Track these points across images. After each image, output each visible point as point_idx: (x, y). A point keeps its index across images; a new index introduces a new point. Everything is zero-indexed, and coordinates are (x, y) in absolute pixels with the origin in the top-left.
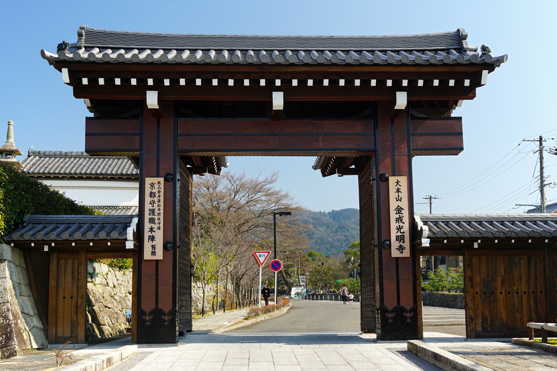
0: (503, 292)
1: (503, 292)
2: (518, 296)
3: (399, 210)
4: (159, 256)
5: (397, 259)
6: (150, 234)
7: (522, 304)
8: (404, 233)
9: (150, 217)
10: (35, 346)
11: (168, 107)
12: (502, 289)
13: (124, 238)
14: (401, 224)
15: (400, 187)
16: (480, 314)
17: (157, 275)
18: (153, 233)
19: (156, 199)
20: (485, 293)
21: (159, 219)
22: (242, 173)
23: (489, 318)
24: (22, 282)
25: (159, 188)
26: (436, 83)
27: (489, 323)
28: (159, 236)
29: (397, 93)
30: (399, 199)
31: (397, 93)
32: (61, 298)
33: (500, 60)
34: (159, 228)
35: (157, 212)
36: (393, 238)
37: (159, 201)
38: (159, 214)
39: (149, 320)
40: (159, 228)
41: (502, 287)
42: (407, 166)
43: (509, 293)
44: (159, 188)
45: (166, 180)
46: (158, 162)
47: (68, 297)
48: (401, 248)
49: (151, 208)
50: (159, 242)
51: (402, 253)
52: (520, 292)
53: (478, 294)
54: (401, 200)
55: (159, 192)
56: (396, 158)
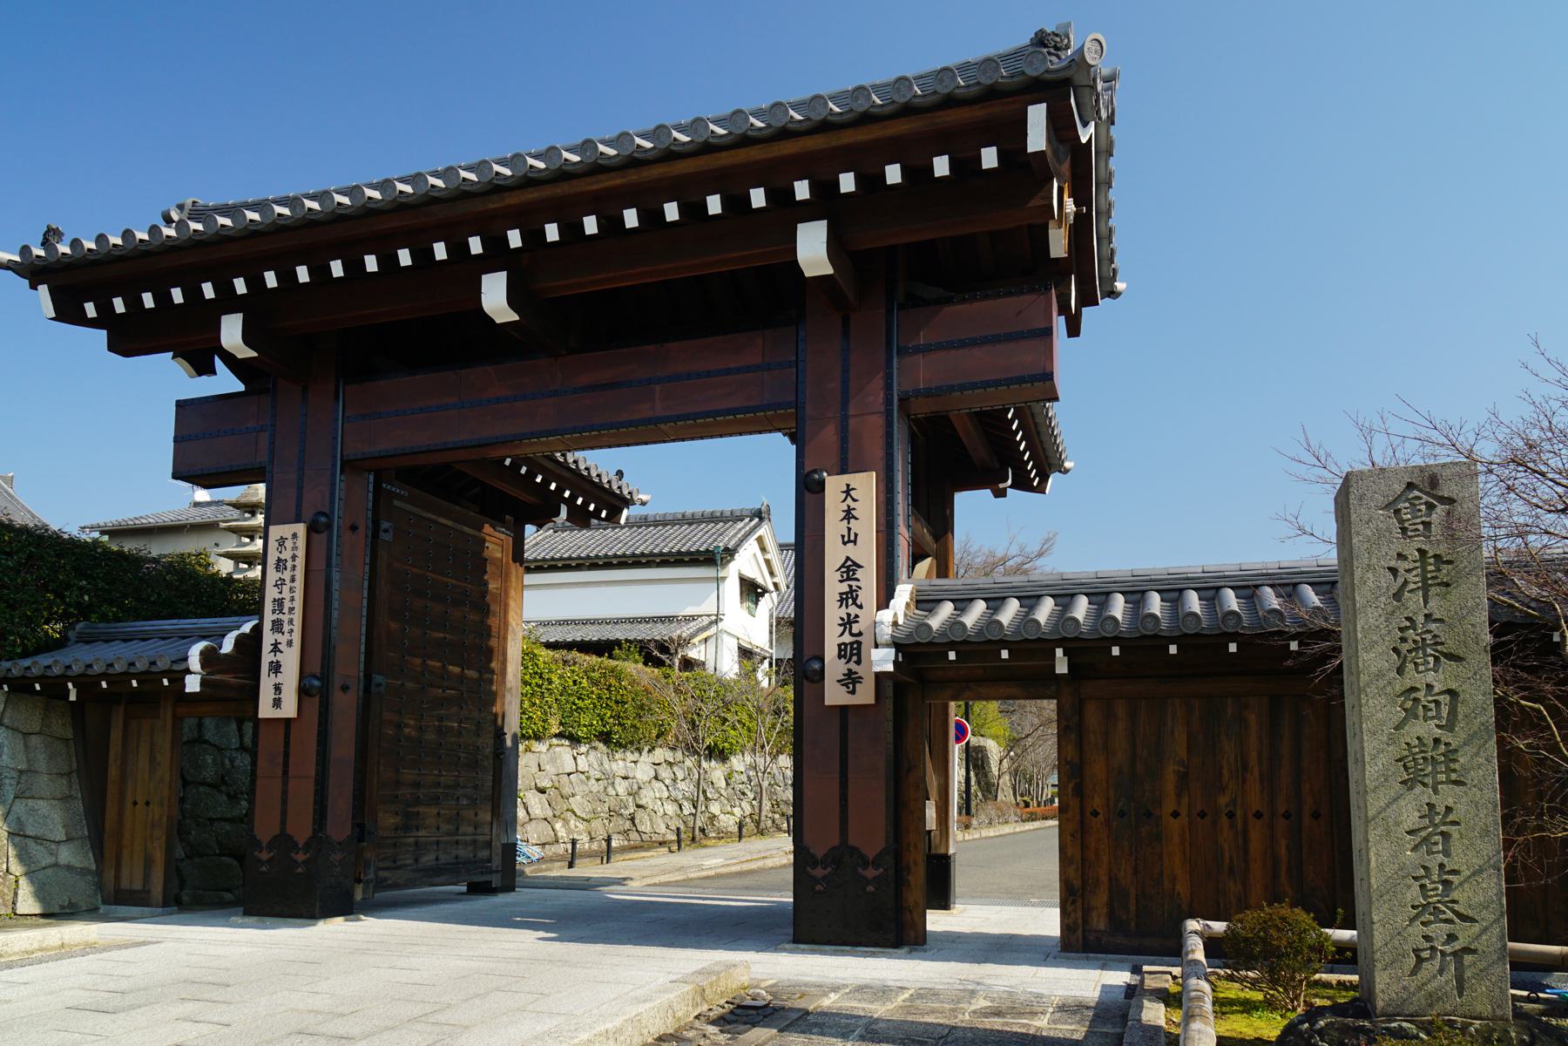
0: (1184, 811)
1: (1184, 811)
2: (1232, 826)
3: (850, 569)
4: (289, 709)
5: (844, 710)
6: (271, 657)
7: (1246, 851)
8: (860, 634)
9: (275, 617)
10: (36, 909)
11: (412, 363)
12: (1179, 803)
13: (181, 667)
14: (853, 610)
15: (853, 504)
16: (1104, 879)
17: (286, 755)
18: (279, 657)
19: (287, 575)
20: (1122, 814)
21: (291, 622)
22: (1034, 548)
23: (1133, 892)
24: (42, 764)
25: (295, 548)
26: (893, 174)
27: (1133, 908)
28: (291, 660)
29: (825, 223)
30: (849, 539)
31: (825, 223)
32: (129, 804)
34: (290, 643)
35: (287, 604)
36: (831, 651)
37: (293, 580)
38: (291, 609)
39: (824, 878)
40: (290, 643)
41: (1179, 795)
42: (881, 443)
43: (1202, 815)
44: (295, 548)
45: (311, 530)
46: (300, 488)
47: (141, 802)
48: (851, 680)
49: (278, 596)
50: (290, 677)
51: (853, 692)
52: (1239, 813)
53: (1101, 817)
54: (855, 542)
55: (294, 557)
56: (852, 422)
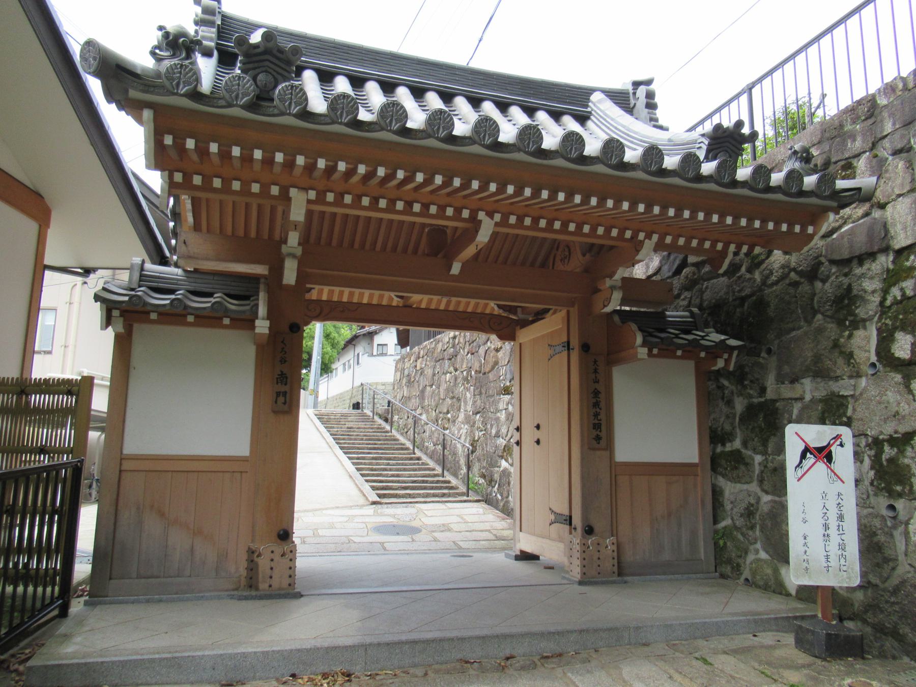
14: (598, 410)
33: (161, 28)
